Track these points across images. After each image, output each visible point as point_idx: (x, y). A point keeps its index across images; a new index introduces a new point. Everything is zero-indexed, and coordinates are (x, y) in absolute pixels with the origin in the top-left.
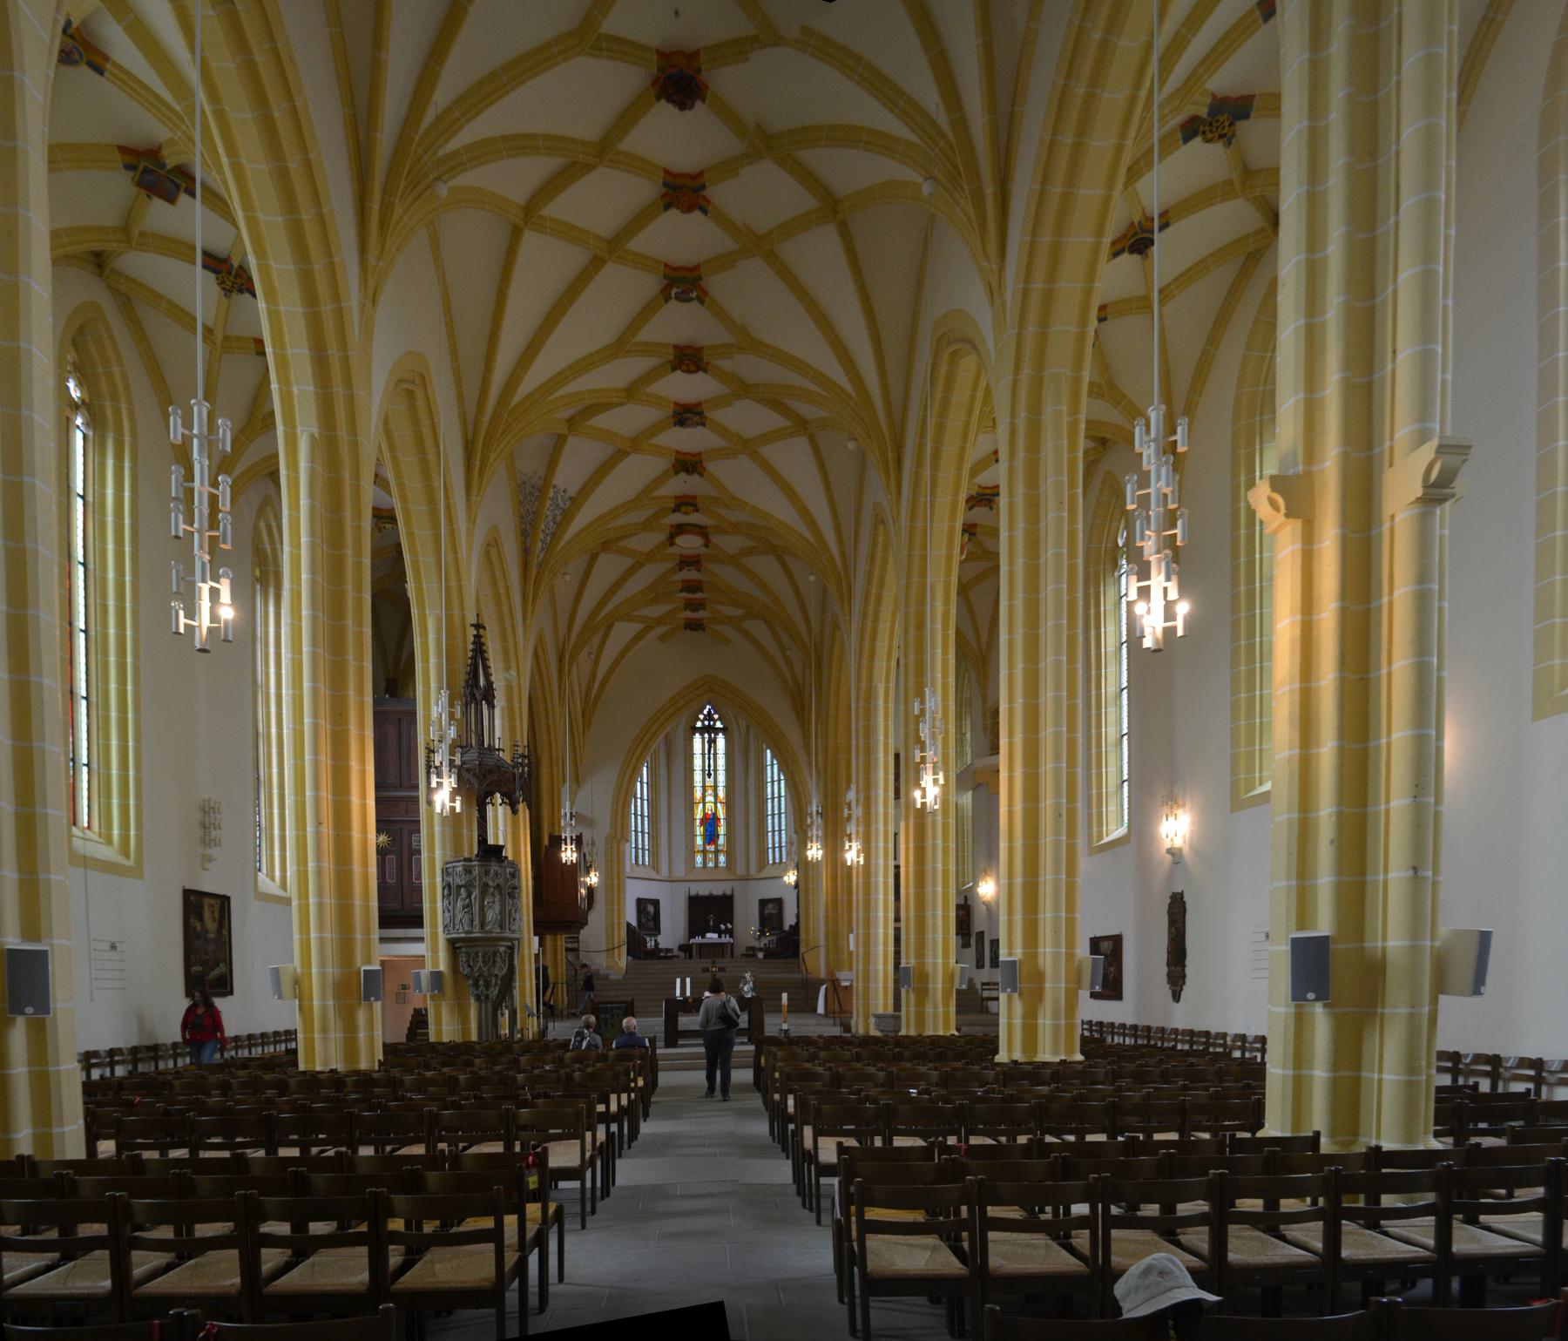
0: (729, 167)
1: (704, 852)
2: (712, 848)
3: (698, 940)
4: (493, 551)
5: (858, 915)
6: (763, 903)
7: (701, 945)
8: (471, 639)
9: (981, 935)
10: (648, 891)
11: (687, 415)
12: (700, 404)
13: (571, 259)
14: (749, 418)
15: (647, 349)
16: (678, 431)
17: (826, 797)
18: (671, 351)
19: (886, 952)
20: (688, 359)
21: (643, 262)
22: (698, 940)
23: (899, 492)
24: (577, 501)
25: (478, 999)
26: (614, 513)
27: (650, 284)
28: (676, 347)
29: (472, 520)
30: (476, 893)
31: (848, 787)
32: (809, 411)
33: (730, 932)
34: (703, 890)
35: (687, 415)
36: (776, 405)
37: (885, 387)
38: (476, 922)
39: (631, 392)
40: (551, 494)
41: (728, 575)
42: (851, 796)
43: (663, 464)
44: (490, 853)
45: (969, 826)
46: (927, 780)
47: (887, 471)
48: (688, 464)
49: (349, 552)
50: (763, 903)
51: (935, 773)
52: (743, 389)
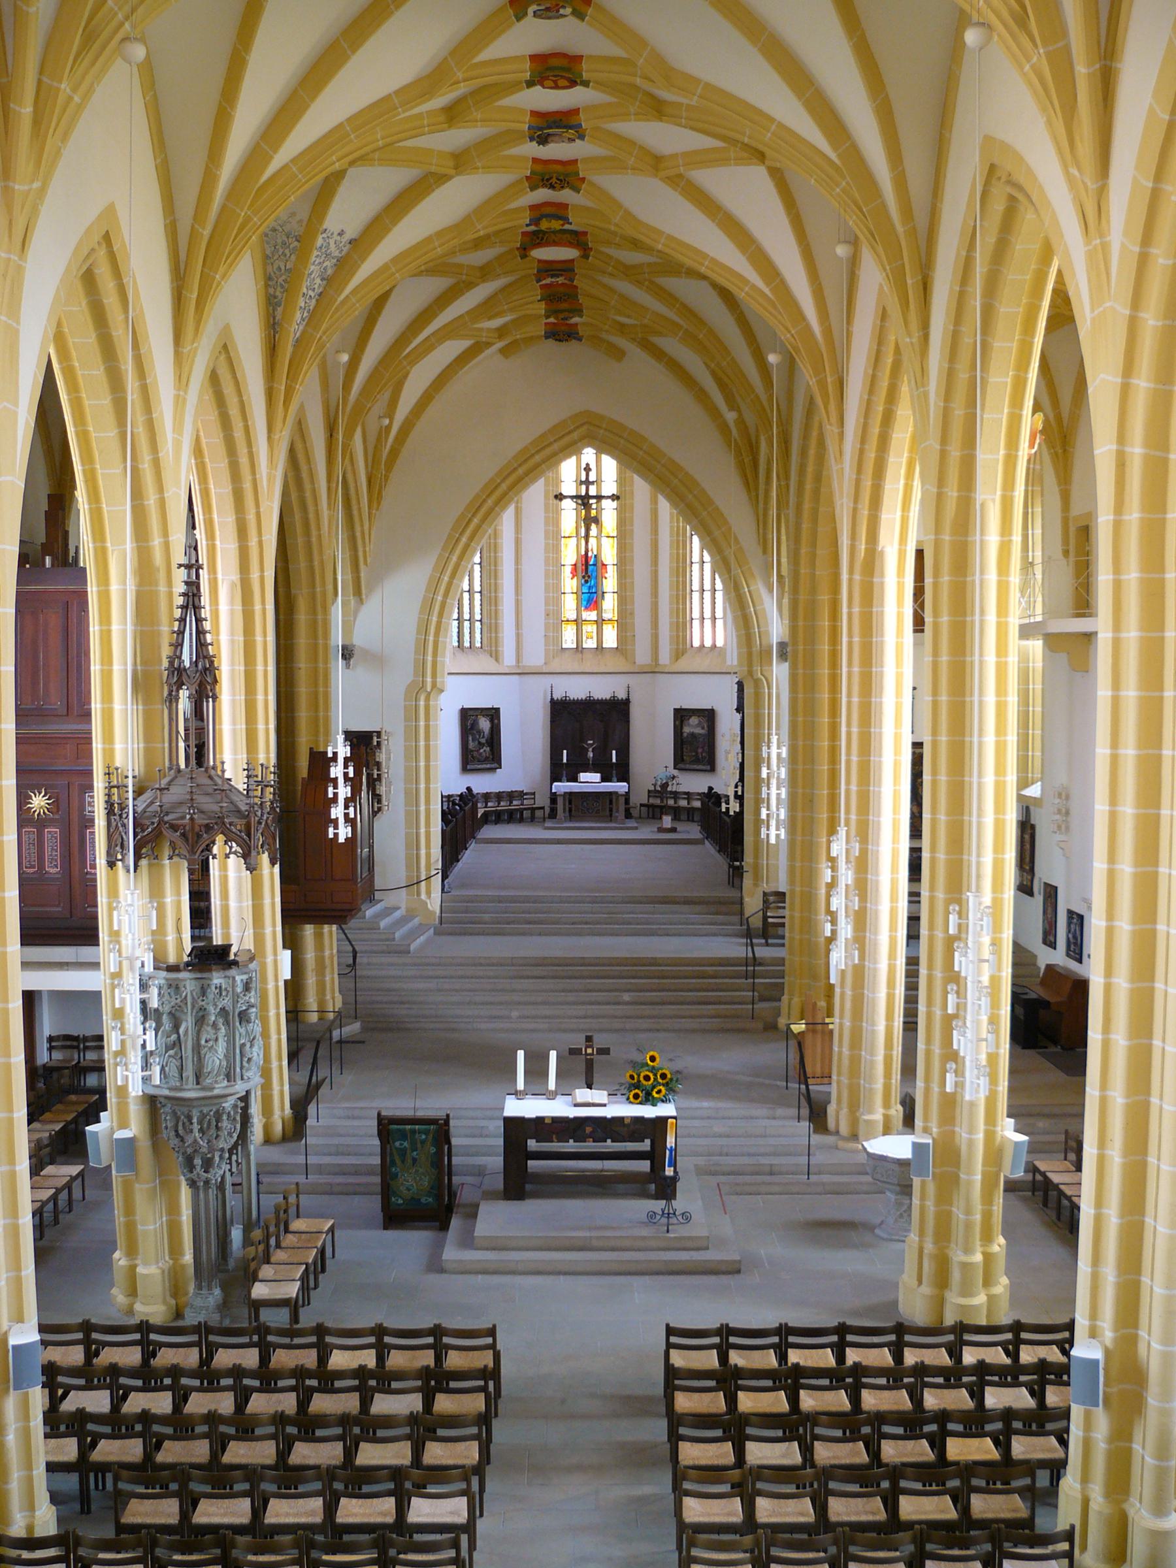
1: (579, 622)
2: (592, 615)
3: (561, 787)
5: (848, 787)
6: (681, 715)
7: (571, 796)
8: (182, 588)
9: (1051, 893)
10: (479, 695)
12: (576, 111)
17: (794, 617)
18: (527, 65)
19: (890, 998)
22: (561, 787)
23: (926, 337)
24: (362, 243)
25: (192, 1184)
28: (534, 58)
29: (180, 359)
30: (187, 1025)
31: (832, 831)
33: (624, 777)
34: (577, 689)
37: (900, 181)
38: (189, 1073)
40: (319, 242)
42: (838, 848)
44: (210, 957)
45: (1036, 686)
50: (681, 715)
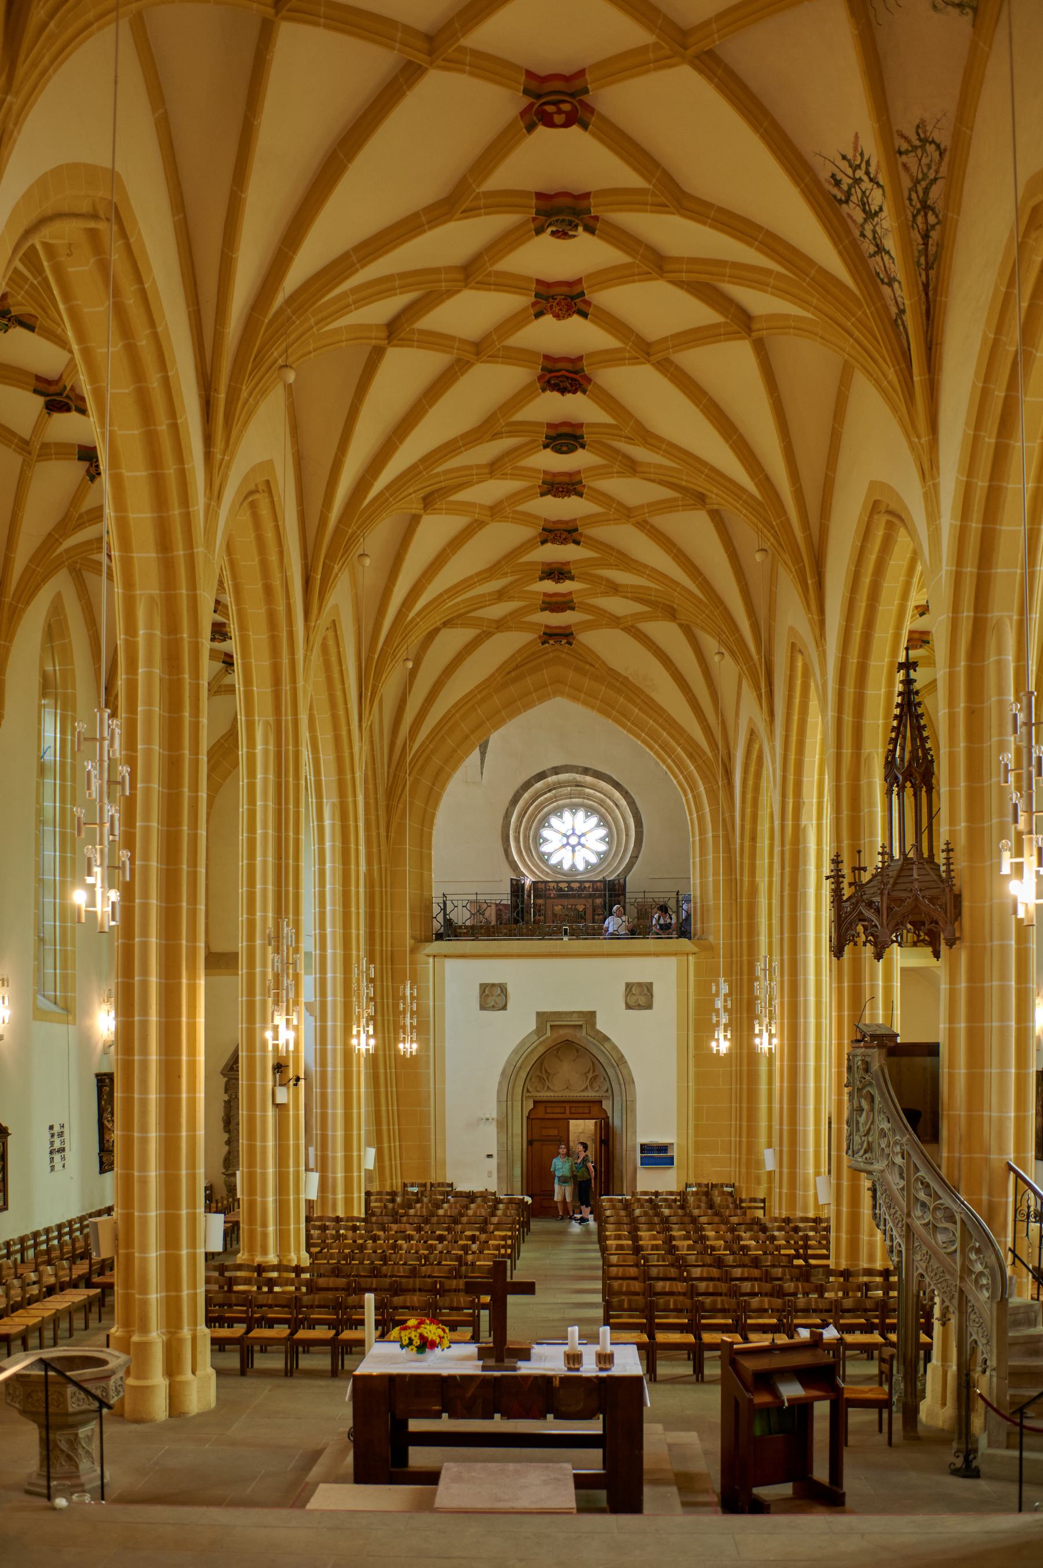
0: (628, 64)
4: (262, 499)
11: (564, 299)
13: (367, 63)
14: (657, 307)
15: (503, 201)
16: (552, 397)
20: (563, 212)
21: (488, 66)
26: (467, 583)
27: (498, 103)
32: (759, 302)
35: (564, 299)
36: (706, 291)
39: (471, 273)
41: (640, 387)
43: (527, 532)
46: (720, 1034)
47: (760, 696)
48: (564, 375)
49: (187, 714)
51: (725, 1031)
52: (655, 263)
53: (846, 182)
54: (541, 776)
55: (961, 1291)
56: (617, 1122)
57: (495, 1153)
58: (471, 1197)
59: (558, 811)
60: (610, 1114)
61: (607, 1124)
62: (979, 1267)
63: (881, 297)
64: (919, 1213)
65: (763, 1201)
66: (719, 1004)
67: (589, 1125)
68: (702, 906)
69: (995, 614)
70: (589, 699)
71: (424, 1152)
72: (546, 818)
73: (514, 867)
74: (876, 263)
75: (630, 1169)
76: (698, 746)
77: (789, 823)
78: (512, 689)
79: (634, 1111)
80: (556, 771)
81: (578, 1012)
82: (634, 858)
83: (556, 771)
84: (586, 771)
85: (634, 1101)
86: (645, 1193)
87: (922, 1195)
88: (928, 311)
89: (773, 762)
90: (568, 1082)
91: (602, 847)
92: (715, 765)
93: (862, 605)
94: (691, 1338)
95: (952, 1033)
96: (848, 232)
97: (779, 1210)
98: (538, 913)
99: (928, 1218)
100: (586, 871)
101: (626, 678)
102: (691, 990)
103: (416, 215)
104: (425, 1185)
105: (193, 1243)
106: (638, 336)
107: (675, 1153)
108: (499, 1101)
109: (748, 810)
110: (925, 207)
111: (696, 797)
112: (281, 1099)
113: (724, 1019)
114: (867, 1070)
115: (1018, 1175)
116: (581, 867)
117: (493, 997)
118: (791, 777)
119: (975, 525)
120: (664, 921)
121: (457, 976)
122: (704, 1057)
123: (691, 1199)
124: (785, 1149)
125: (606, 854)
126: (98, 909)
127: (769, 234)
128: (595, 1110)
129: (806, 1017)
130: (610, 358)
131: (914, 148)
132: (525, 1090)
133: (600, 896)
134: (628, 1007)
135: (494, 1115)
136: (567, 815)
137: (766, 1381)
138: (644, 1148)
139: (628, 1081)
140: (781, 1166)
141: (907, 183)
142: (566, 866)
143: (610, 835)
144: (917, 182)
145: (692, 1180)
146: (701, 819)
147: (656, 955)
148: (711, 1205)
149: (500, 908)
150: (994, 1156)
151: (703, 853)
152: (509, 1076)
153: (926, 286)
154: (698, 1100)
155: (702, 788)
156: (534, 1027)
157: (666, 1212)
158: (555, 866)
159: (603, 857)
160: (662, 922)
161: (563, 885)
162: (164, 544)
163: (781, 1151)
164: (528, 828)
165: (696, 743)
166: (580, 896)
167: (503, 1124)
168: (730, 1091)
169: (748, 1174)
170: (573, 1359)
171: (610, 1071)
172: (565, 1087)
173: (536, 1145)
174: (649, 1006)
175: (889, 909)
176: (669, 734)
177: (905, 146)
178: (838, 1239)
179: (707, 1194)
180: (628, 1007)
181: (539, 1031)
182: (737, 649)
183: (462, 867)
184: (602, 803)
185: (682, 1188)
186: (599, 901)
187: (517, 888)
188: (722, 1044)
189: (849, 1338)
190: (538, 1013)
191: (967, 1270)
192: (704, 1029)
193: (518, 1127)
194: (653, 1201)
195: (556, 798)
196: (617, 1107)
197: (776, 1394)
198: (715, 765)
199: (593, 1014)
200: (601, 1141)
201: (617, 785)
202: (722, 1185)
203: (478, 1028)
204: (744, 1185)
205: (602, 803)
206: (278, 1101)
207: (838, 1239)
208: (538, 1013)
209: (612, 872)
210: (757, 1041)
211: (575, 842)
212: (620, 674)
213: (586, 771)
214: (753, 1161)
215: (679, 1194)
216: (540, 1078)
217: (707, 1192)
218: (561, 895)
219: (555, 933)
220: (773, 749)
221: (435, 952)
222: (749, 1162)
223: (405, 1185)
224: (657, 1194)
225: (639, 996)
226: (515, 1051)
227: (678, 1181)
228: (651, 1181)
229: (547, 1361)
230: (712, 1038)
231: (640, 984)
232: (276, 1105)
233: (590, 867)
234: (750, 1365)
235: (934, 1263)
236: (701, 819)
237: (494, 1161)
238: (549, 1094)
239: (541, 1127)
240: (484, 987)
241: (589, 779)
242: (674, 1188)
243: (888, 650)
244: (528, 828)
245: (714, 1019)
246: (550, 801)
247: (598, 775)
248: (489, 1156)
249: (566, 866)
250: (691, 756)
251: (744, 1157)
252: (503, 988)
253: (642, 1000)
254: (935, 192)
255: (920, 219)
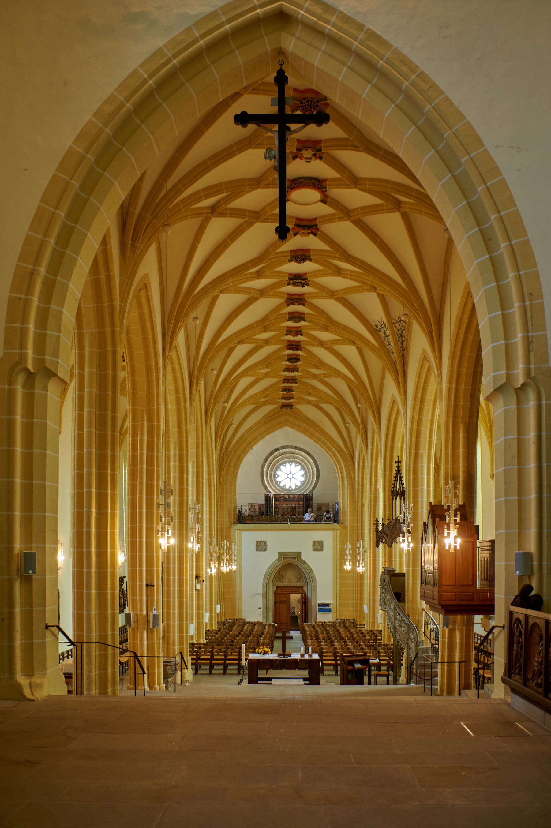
12: (306, 274)
53: (379, 327)
54: (277, 450)
55: (408, 644)
56: (309, 595)
57: (262, 607)
58: (254, 624)
59: (284, 464)
60: (306, 592)
61: (305, 596)
62: (412, 637)
63: (390, 356)
64: (397, 622)
65: (365, 625)
66: (347, 552)
67: (298, 596)
68: (343, 511)
69: (421, 452)
70: (299, 428)
71: (233, 607)
72: (279, 466)
73: (266, 488)
74: (388, 347)
75: (314, 613)
76: (341, 448)
77: (373, 487)
78: (269, 424)
79: (316, 590)
80: (283, 447)
81: (294, 552)
82: (316, 484)
83: (283, 447)
84: (296, 448)
85: (316, 587)
86: (320, 622)
87: (398, 617)
88: (404, 362)
89: (368, 464)
90: (290, 579)
91: (303, 479)
92: (349, 457)
93: (391, 428)
94: (334, 662)
95: (408, 571)
96: (381, 339)
97: (368, 628)
98: (276, 510)
99: (399, 623)
100: (296, 489)
101: (313, 421)
102: (338, 544)
103: (252, 324)
104: (234, 619)
105: (187, 632)
106: (319, 340)
107: (332, 607)
108: (263, 587)
109: (360, 475)
110: (402, 336)
111: (341, 468)
112: (198, 588)
113: (349, 558)
114: (385, 581)
115: (425, 612)
116: (293, 487)
117: (261, 546)
118: (374, 471)
119: (415, 428)
120: (328, 515)
121: (247, 537)
122: (342, 571)
123: (338, 624)
124: (371, 605)
125: (304, 482)
126: (194, 548)
127: (358, 333)
128: (301, 590)
129: (378, 557)
130: (329, 219)
131: (398, 322)
132: (273, 582)
133: (302, 501)
134: (314, 550)
135: (261, 592)
136: (288, 465)
137: (351, 663)
138: (320, 605)
139: (314, 579)
140: (370, 611)
141: (396, 330)
142: (287, 487)
143: (306, 474)
144: (399, 330)
145: (338, 618)
146: (342, 476)
147: (325, 530)
148: (345, 626)
149: (260, 506)
150: (419, 606)
151: (343, 490)
152: (267, 577)
153: (403, 355)
154: (341, 586)
155: (343, 465)
156: (277, 558)
157: (328, 628)
158: (283, 487)
159: (303, 483)
160: (327, 516)
161: (287, 496)
162: (179, 426)
163: (370, 606)
164: (271, 471)
165: (340, 446)
166: (293, 501)
167: (265, 596)
168: (351, 584)
169: (360, 615)
170: (302, 655)
171: (306, 575)
172: (289, 582)
173: (277, 604)
174: (322, 550)
175: (390, 535)
176: (330, 443)
177: (395, 322)
178: (384, 634)
179: (343, 622)
180: (314, 550)
181: (279, 559)
182: (355, 422)
183: (247, 493)
184: (302, 461)
185: (334, 620)
186: (301, 503)
187: (267, 498)
188: (348, 567)
189: (382, 662)
190: (279, 553)
191: (409, 638)
192: (343, 561)
193: (270, 597)
194: (323, 625)
195: (283, 458)
196: (309, 589)
197: (354, 667)
198: (349, 457)
199: (300, 553)
200: (303, 602)
201: (309, 454)
202: (350, 620)
203: (255, 557)
204: (358, 620)
205: (302, 461)
206: (197, 588)
207: (384, 634)
208: (279, 553)
209: (307, 490)
210: (358, 569)
211: (291, 477)
212: (311, 420)
213: (296, 448)
214: (361, 610)
215: (333, 622)
216: (279, 578)
217: (344, 622)
218: (286, 500)
219: (285, 521)
220: (367, 459)
221: (238, 528)
222: (360, 610)
223: (226, 620)
224: (325, 622)
225: (318, 546)
226: (270, 567)
227: (333, 618)
228: (322, 618)
229: (296, 656)
230: (345, 564)
231: (318, 541)
232: (196, 590)
233: (298, 488)
234: (347, 659)
235: (401, 636)
236: (342, 476)
237: (261, 610)
238: (283, 584)
239: (279, 597)
240: (257, 542)
241: (297, 451)
242: (332, 621)
243: (400, 442)
244: (271, 471)
245: (346, 558)
246: (281, 459)
247: (301, 449)
248: (260, 608)
249: (287, 487)
250: (339, 452)
251: (359, 609)
252: (265, 543)
253: (319, 548)
254: (404, 332)
255: (400, 339)
